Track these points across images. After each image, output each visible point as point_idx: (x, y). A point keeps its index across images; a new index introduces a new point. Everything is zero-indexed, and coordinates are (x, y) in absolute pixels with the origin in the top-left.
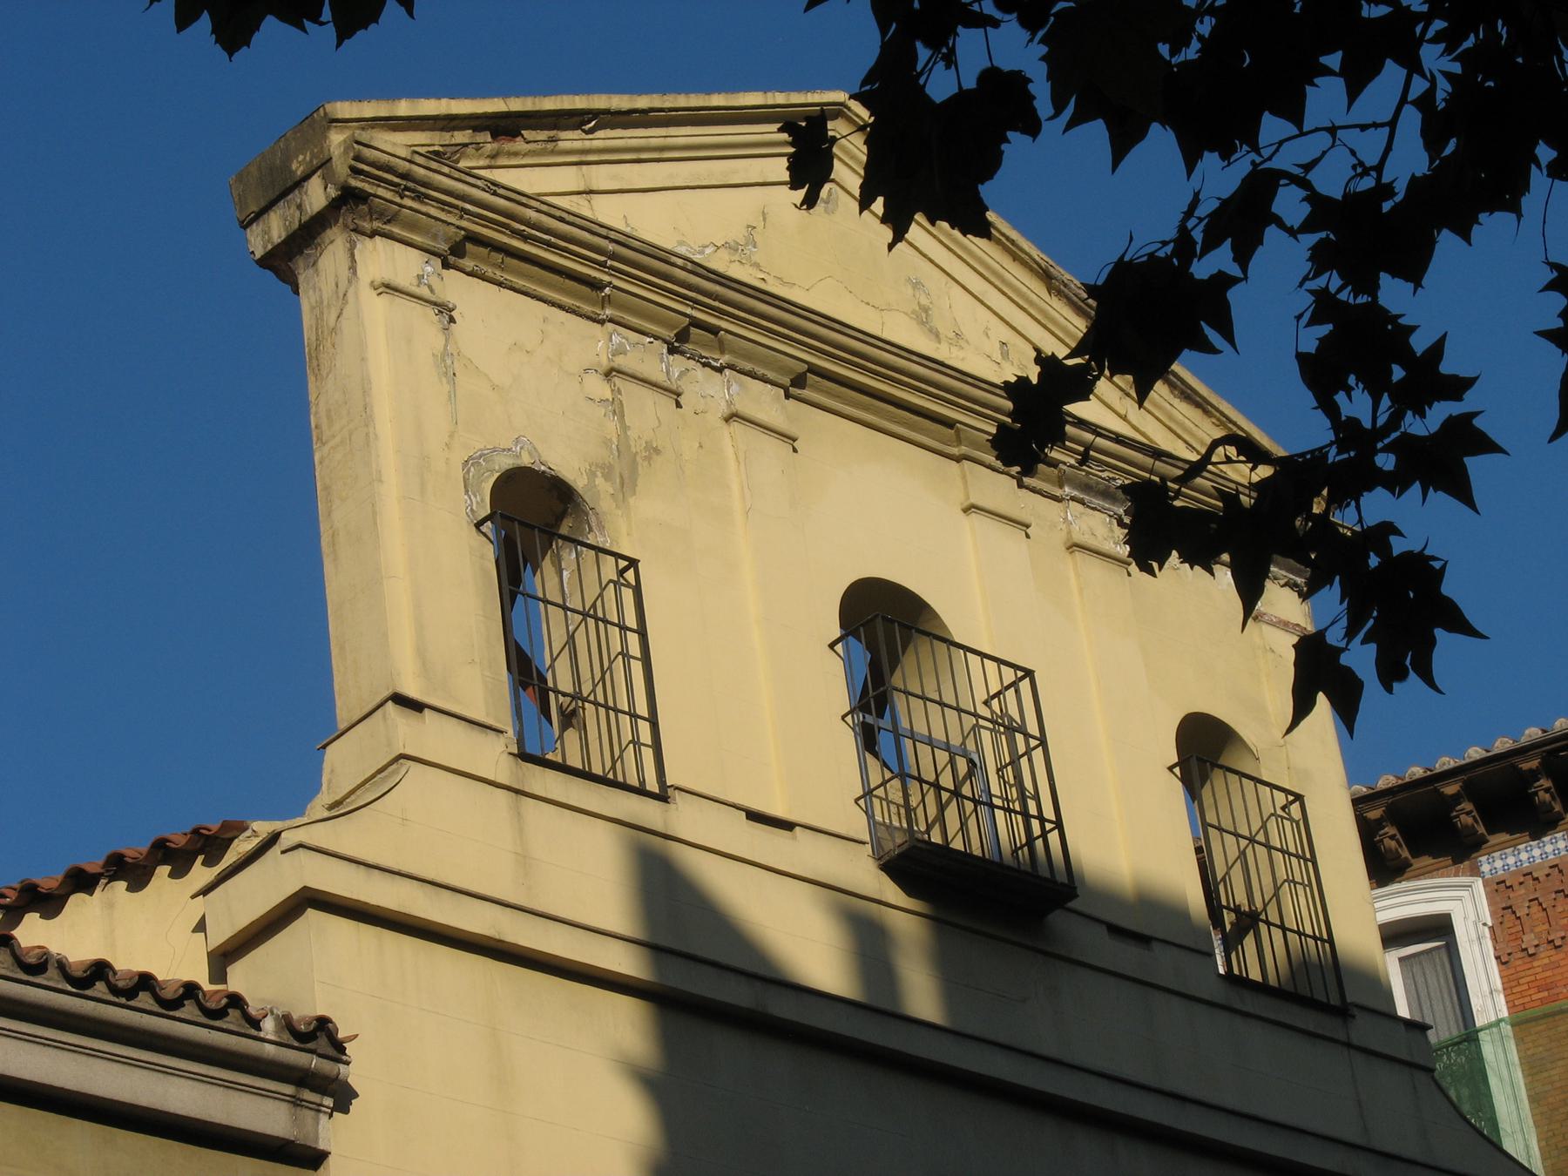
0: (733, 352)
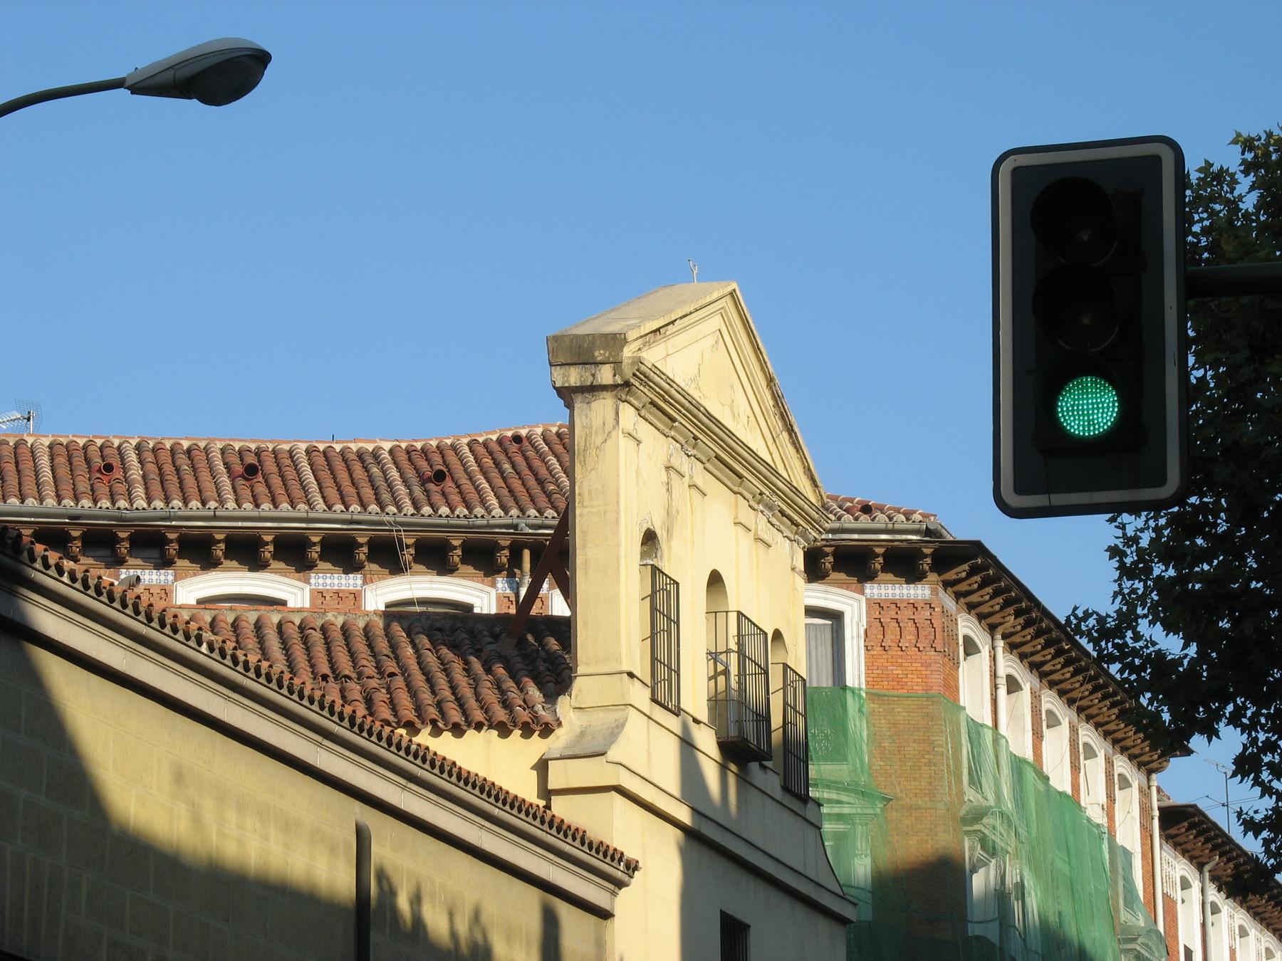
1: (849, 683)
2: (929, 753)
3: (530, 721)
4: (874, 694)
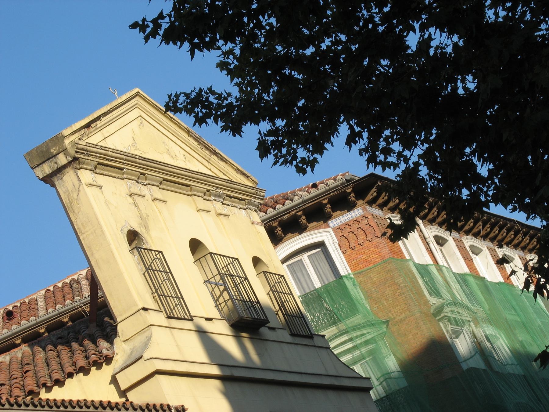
0: (149, 180)
1: (342, 274)
2: (398, 289)
3: (98, 359)
4: (358, 273)
